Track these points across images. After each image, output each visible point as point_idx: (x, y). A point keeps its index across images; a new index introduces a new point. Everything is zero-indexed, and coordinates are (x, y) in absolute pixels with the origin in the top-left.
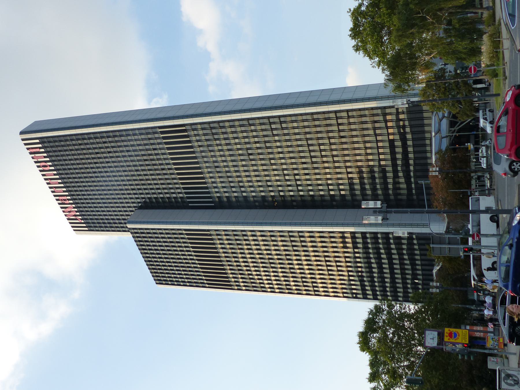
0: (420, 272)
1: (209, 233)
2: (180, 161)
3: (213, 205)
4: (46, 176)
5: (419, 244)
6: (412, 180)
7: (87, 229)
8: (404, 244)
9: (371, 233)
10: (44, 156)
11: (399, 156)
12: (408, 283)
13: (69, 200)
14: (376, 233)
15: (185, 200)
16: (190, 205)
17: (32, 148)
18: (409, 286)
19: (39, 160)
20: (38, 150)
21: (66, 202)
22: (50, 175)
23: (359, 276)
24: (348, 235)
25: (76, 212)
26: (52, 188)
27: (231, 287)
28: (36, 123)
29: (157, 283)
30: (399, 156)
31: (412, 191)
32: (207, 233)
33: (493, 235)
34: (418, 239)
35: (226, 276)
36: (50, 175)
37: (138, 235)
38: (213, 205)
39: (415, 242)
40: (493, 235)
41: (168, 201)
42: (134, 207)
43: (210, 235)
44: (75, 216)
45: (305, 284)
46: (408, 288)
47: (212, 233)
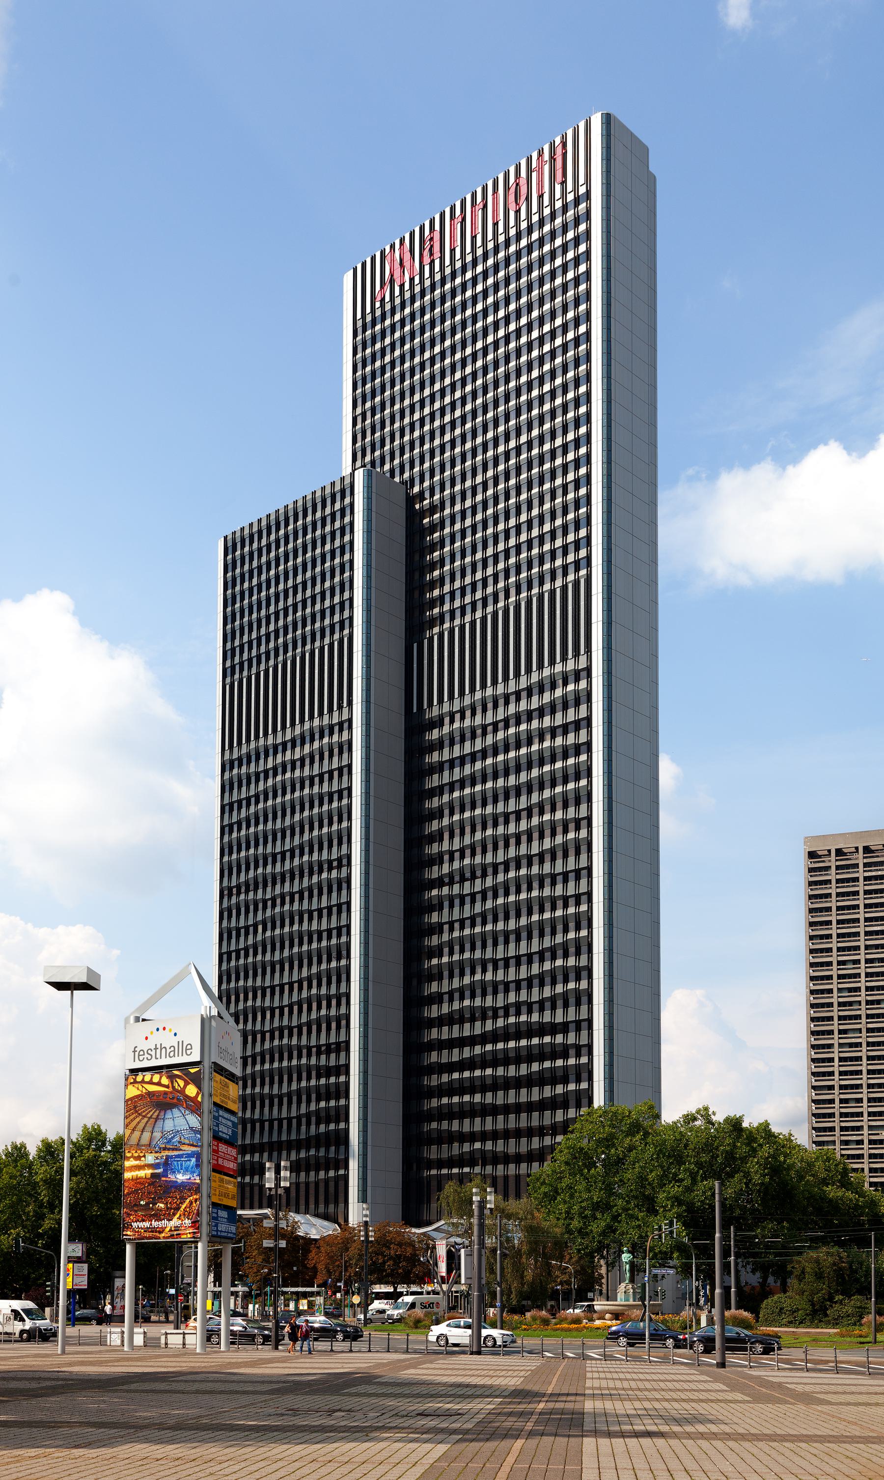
1: (345, 704)
3: (415, 711)
4: (493, 195)
5: (327, 1181)
6: (455, 1171)
7: (359, 316)
8: (252, 1178)
10: (543, 195)
11: (500, 1146)
12: (252, 1156)
16: (415, 645)
17: (564, 156)
19: (534, 175)
21: (426, 253)
24: (583, 712)
27: (227, 748)
28: (640, 151)
29: (226, 538)
30: (500, 1146)
31: (467, 1166)
33: (72, 994)
34: (337, 1178)
37: (345, 490)
38: (415, 711)
39: (332, 1173)
40: (72, 994)
43: (340, 707)
47: (345, 711)
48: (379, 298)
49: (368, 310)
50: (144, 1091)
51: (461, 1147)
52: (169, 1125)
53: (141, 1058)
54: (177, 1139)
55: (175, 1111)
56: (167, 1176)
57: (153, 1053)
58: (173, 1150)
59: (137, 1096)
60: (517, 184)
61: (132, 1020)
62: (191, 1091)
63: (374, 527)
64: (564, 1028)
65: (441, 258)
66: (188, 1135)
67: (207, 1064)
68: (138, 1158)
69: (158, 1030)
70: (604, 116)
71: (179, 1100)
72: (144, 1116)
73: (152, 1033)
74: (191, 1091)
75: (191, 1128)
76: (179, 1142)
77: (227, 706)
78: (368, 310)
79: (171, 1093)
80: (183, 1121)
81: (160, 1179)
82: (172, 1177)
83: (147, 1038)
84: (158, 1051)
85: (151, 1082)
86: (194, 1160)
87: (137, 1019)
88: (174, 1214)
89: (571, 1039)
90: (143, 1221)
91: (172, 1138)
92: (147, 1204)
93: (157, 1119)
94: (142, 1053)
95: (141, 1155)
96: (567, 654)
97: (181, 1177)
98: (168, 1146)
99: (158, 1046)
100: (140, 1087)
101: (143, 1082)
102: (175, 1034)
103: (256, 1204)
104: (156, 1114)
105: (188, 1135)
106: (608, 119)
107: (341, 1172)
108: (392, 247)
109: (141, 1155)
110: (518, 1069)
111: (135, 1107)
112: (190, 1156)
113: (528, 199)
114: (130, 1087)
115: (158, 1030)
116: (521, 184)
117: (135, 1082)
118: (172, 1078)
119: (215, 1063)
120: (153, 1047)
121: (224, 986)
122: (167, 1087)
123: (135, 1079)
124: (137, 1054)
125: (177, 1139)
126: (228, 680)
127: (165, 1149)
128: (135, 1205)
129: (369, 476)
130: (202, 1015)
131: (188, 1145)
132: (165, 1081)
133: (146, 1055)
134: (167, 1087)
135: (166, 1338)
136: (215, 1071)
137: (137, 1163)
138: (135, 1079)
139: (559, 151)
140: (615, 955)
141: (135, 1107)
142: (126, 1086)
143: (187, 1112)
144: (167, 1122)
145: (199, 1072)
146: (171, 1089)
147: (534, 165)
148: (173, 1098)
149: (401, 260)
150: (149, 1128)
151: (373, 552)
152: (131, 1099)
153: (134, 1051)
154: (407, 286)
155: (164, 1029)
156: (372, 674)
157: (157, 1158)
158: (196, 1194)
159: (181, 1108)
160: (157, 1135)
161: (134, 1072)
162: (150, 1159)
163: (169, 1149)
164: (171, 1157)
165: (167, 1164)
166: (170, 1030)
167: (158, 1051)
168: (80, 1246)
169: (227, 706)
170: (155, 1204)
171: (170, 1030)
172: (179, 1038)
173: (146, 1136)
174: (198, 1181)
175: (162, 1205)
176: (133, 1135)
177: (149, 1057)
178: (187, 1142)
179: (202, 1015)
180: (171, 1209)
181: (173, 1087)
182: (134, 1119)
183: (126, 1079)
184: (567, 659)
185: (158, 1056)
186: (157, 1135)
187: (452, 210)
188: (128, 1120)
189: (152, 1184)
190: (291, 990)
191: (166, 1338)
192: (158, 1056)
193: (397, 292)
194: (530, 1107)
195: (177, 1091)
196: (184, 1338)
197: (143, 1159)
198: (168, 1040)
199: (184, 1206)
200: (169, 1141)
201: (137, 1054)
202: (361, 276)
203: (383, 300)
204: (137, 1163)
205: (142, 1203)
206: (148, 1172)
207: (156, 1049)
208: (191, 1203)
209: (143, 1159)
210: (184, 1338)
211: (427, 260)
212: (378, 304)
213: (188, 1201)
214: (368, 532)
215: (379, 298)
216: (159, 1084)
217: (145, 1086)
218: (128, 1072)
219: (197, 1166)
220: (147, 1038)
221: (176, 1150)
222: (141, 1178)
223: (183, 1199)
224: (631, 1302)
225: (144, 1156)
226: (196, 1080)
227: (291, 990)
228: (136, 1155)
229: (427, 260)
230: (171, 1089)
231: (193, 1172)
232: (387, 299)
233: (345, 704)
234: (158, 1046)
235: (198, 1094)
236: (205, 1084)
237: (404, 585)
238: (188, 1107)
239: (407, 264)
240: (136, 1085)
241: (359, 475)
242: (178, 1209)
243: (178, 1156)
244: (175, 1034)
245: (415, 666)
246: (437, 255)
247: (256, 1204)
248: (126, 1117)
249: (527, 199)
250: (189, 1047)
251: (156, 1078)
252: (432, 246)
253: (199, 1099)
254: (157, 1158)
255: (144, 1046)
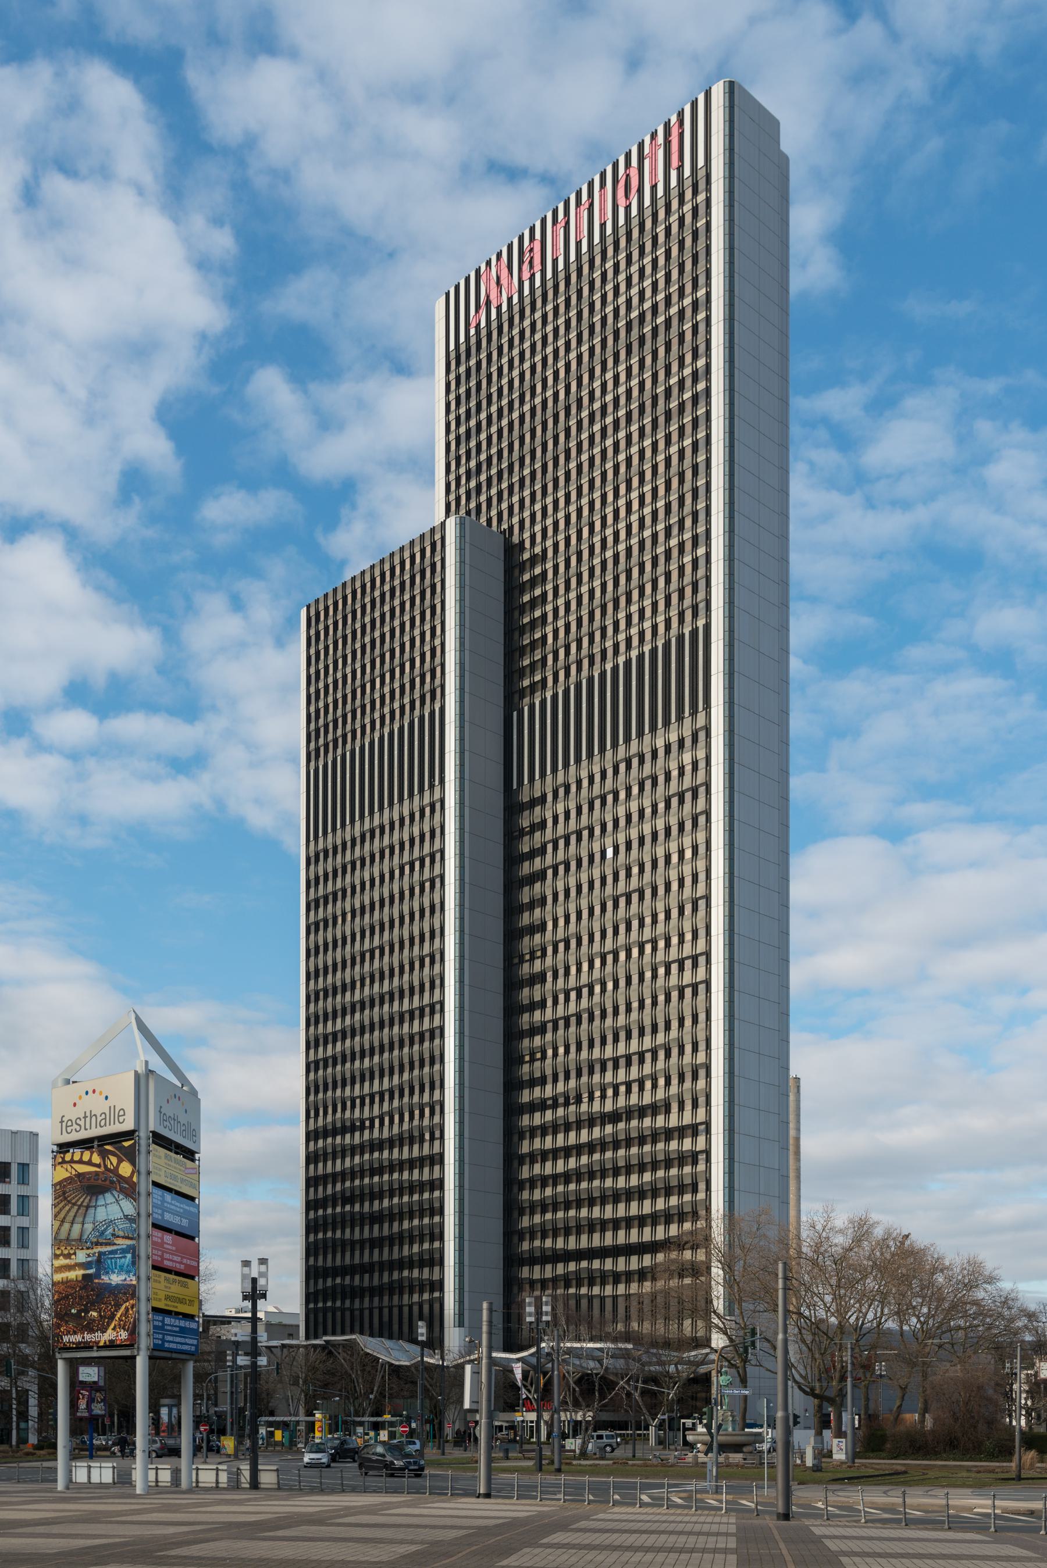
0: (366, 1304)
1: (437, 783)
2: (660, 671)
3: (515, 787)
7: (452, 347)
9: (442, 1200)
13: (530, 279)
14: (441, 1212)
15: (526, 700)
16: (515, 713)
17: (681, 135)
18: (338, 1280)
19: (647, 162)
20: (675, 162)
21: (526, 266)
22: (602, 210)
23: (362, 1122)
25: (499, 308)
26: (565, 215)
32: (700, 701)
35: (329, 830)
36: (602, 210)
37: (434, 540)
39: (426, 1296)
41: (525, 643)
42: (511, 528)
44: (488, 303)
45: (407, 868)
46: (334, 1279)
47: (437, 789)
48: (473, 324)
49: (462, 339)
50: (74, 1172)
51: (566, 1266)
52: (101, 1214)
53: (69, 1130)
54: (110, 1231)
55: (108, 1195)
56: (100, 1278)
57: (82, 1123)
58: (106, 1244)
59: (65, 1180)
60: (628, 176)
61: (60, 1082)
62: (125, 1169)
63: (467, 582)
64: (681, 1132)
65: (542, 270)
66: (123, 1225)
67: (143, 1134)
68: (68, 1256)
69: (87, 1093)
70: (727, 84)
71: (112, 1182)
72: (74, 1204)
73: (80, 1098)
74: (125, 1169)
75: (126, 1217)
76: (113, 1235)
77: (312, 793)
78: (462, 339)
79: (103, 1173)
80: (116, 1207)
81: (92, 1282)
82: (105, 1278)
83: (75, 1105)
84: (88, 1119)
85: (81, 1162)
86: (129, 1256)
87: (67, 1082)
88: (109, 1325)
89: (687, 1144)
90: (75, 1333)
91: (105, 1230)
92: (79, 1312)
93: (88, 1207)
94: (69, 1123)
95: (72, 1252)
96: (683, 712)
97: (116, 1279)
98: (101, 1241)
99: (88, 1114)
100: (69, 1168)
101: (72, 1161)
102: (107, 1098)
103: (348, 1329)
104: (87, 1201)
105: (123, 1225)
106: (731, 88)
107: (436, 1294)
108: (489, 263)
109: (72, 1252)
110: (628, 1180)
111: (64, 1193)
112: (124, 1251)
113: (640, 191)
114: (58, 1168)
115: (87, 1093)
116: (632, 175)
117: (64, 1162)
118: (104, 1154)
119: (153, 1132)
120: (82, 1116)
121: (312, 1098)
122: (98, 1166)
123: (63, 1158)
124: (64, 1124)
125: (110, 1231)
126: (312, 764)
127: (97, 1244)
128: (66, 1314)
129: (462, 524)
130: (136, 1072)
131: (123, 1237)
132: (96, 1159)
133: (75, 1126)
134: (98, 1166)
135: (197, 1474)
136: (154, 1142)
137: (67, 1262)
138: (63, 1158)
139: (675, 132)
140: (736, 1051)
141: (64, 1193)
142: (54, 1166)
143: (121, 1197)
144: (99, 1209)
145: (134, 1145)
146: (102, 1169)
147: (647, 151)
148: (105, 1180)
149: (498, 278)
150: (79, 1219)
151: (467, 610)
152: (60, 1183)
153: (62, 1122)
154: (504, 308)
155: (94, 1091)
156: (467, 747)
157: (89, 1256)
158: (132, 1299)
159: (114, 1192)
160: (89, 1227)
161: (61, 1146)
162: (81, 1256)
163: (101, 1244)
164: (104, 1253)
165: (99, 1262)
166: (101, 1093)
167: (88, 1119)
168: (96, 1369)
169: (312, 793)
170: (86, 1312)
171: (101, 1093)
172: (110, 1102)
173: (77, 1227)
174: (134, 1282)
175: (95, 1314)
176: (63, 1229)
177: (78, 1128)
178: (121, 1233)
179: (136, 1072)
180: (105, 1317)
181: (105, 1166)
182: (64, 1207)
183: (54, 1158)
184: (683, 718)
185: (88, 1126)
186: (89, 1227)
187: (555, 212)
188: (57, 1209)
189: (84, 1288)
190: (382, 1100)
191: (197, 1474)
192: (88, 1126)
193: (494, 316)
194: (641, 1221)
195: (109, 1170)
196: (217, 1475)
197: (73, 1257)
198: (99, 1106)
199: (118, 1315)
200: (103, 1233)
201: (64, 1124)
202: (454, 299)
203: (478, 325)
204: (67, 1262)
205: (73, 1311)
206: (80, 1273)
207: (85, 1117)
208: (127, 1309)
209: (73, 1257)
210: (217, 1475)
211: (526, 275)
212: (472, 332)
213: (124, 1307)
214: (460, 587)
215: (473, 324)
216: (89, 1163)
217: (75, 1166)
218: (55, 1148)
219: (134, 1263)
220: (75, 1105)
221: (110, 1244)
222: (71, 1281)
223: (118, 1306)
224: (737, 1432)
225: (75, 1254)
226: (131, 1155)
227: (382, 1100)
228: (66, 1252)
229: (526, 275)
230: (102, 1169)
231: (128, 1272)
232: (483, 324)
233: (437, 783)
234: (88, 1114)
235: (133, 1173)
236: (141, 1160)
237: (502, 647)
238: (122, 1190)
239: (504, 281)
240: (65, 1166)
241: (451, 524)
242: (112, 1317)
243: (111, 1252)
244: (107, 1098)
245: (515, 737)
246: (537, 266)
247: (348, 1329)
248: (54, 1206)
249: (639, 191)
250: (122, 1113)
251: (86, 1156)
252: (532, 258)
253: (135, 1179)
254: (89, 1256)
255: (73, 1114)
